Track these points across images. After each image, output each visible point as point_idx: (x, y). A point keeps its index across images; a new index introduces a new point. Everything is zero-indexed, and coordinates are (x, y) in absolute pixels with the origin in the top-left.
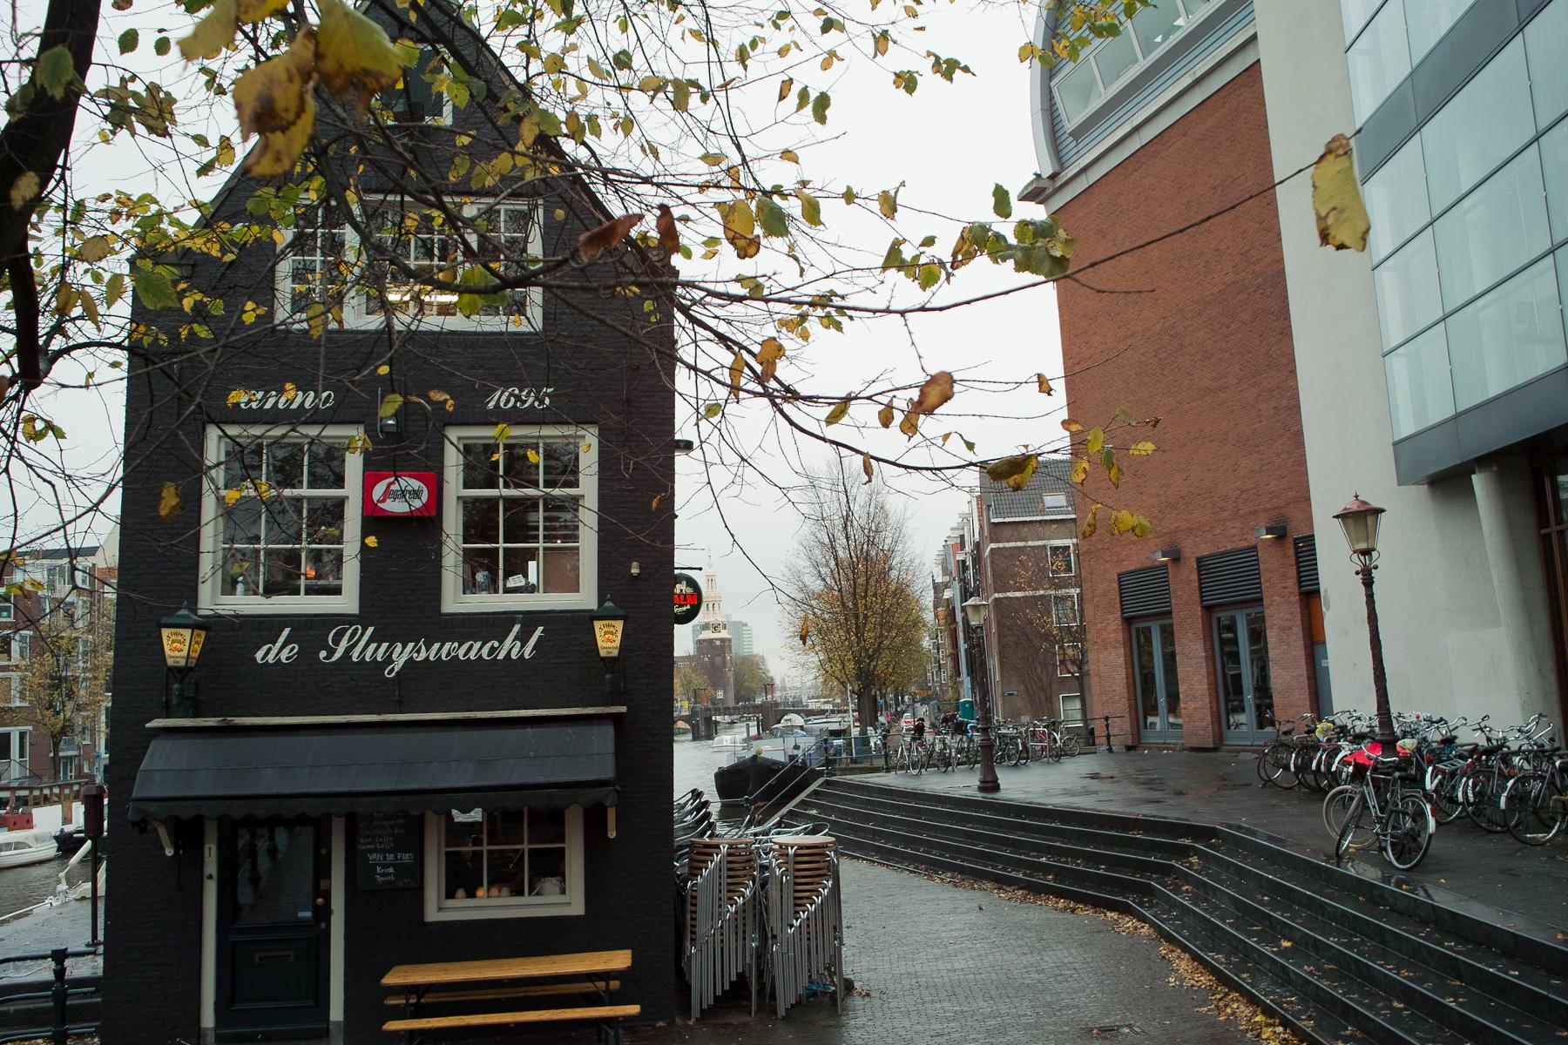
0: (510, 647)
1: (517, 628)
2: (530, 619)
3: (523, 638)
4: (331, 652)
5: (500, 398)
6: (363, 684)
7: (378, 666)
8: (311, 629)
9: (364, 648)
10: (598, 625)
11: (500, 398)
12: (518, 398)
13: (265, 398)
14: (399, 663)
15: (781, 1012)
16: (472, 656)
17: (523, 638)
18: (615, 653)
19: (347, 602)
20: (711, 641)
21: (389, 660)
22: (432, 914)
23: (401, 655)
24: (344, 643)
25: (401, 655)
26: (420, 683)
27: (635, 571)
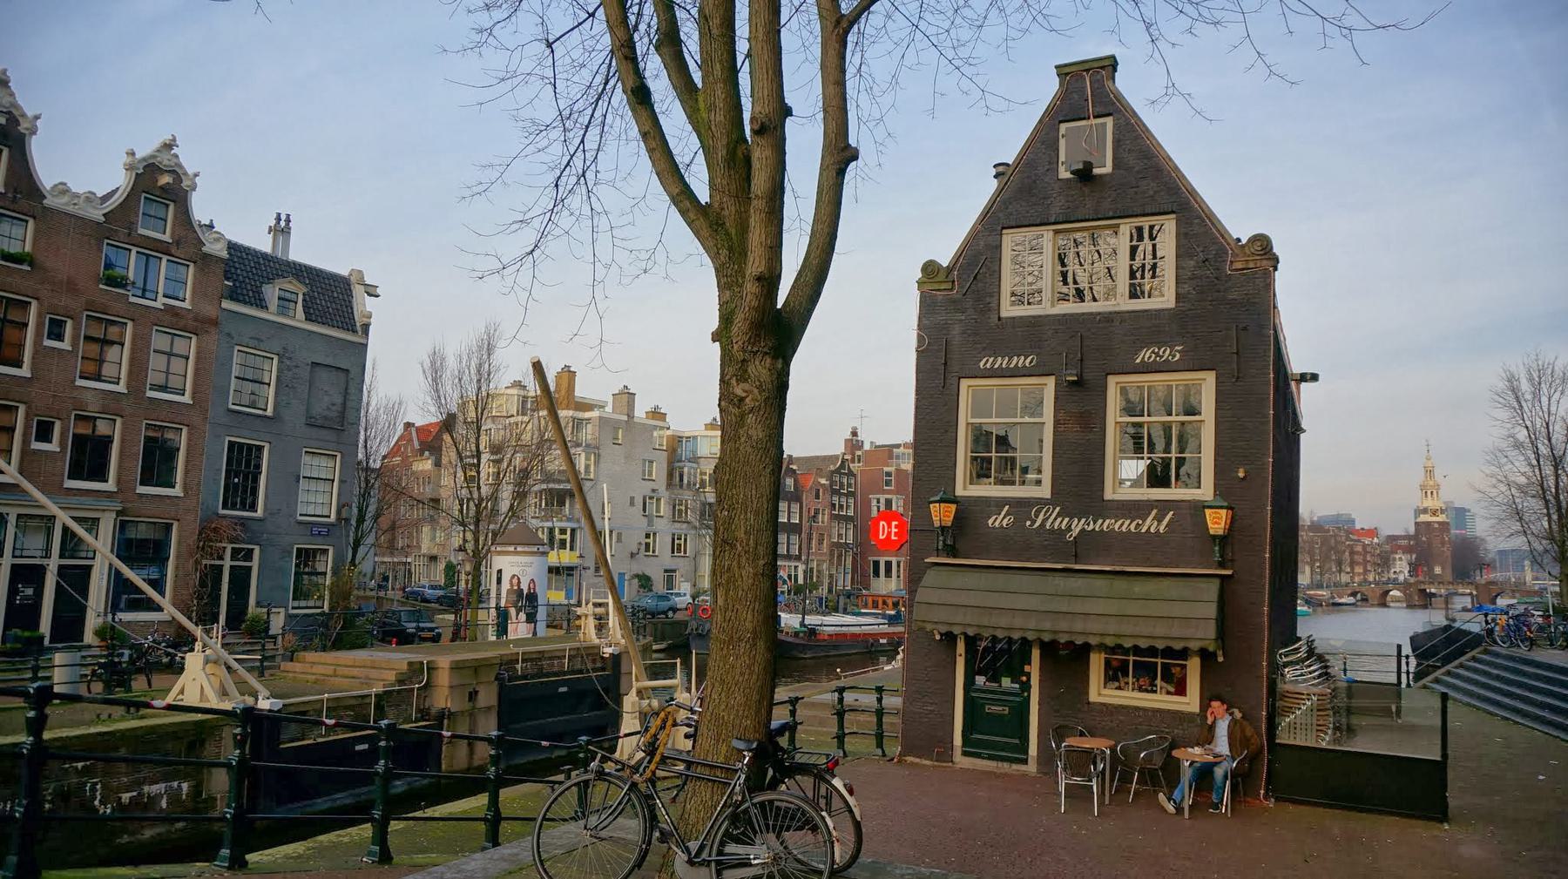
0: (1149, 524)
1: (1154, 512)
2: (1164, 506)
4: (1034, 522)
5: (1146, 355)
6: (1055, 543)
7: (1061, 533)
8: (1021, 507)
9: (1054, 520)
10: (1208, 512)
11: (1146, 355)
12: (1157, 355)
13: (994, 363)
14: (1075, 532)
15: (1036, 654)
16: (1124, 529)
18: (1221, 532)
19: (1045, 491)
20: (1429, 524)
21: (1069, 529)
22: (1093, 697)
23: (1077, 526)
24: (1041, 517)
25: (1077, 526)
26: (1086, 545)
27: (1241, 475)
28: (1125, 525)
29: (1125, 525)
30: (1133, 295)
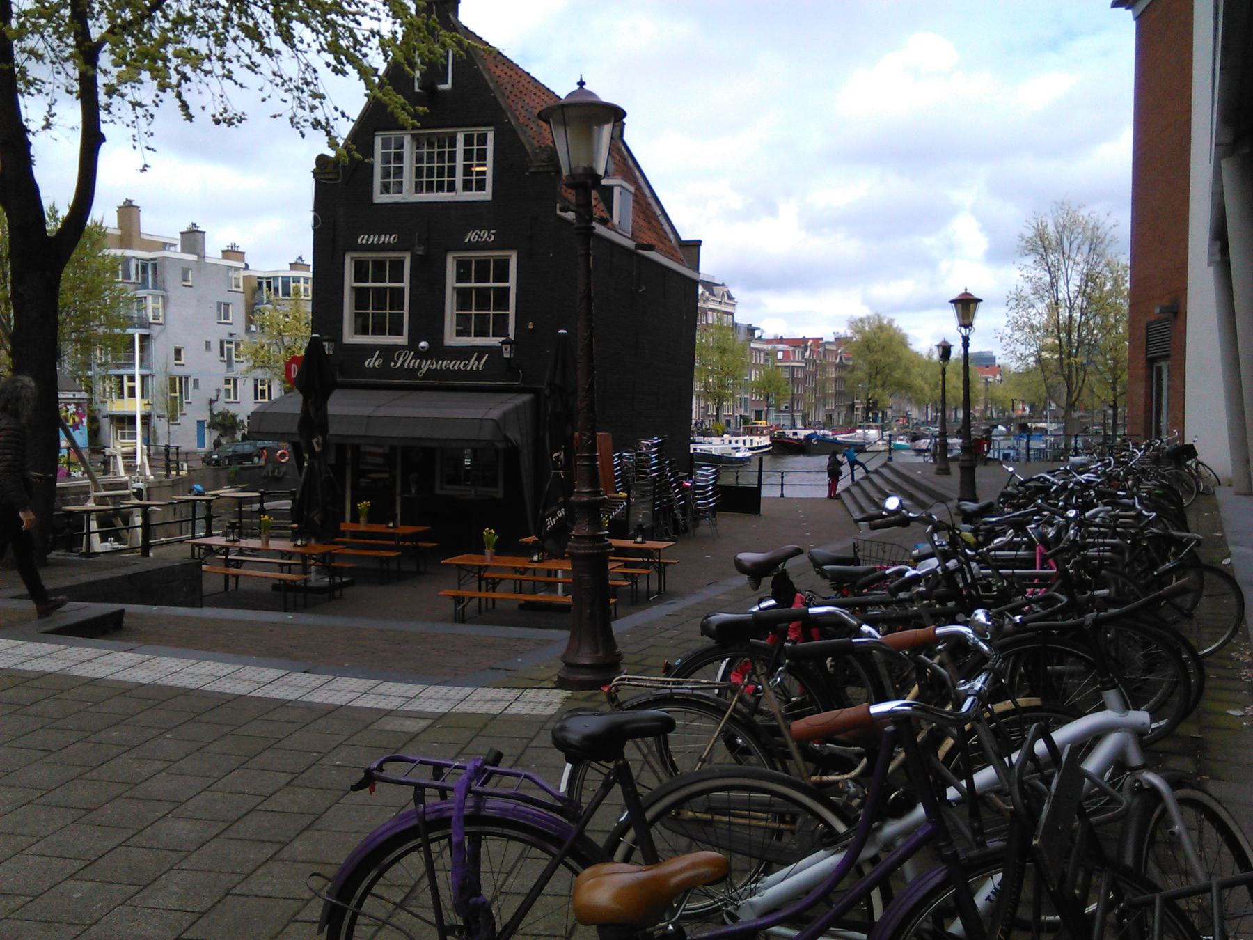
0: (473, 364)
2: (481, 350)
3: (479, 360)
5: (472, 236)
11: (472, 236)
17: (479, 360)
28: (457, 365)
29: (457, 365)
30: (467, 186)
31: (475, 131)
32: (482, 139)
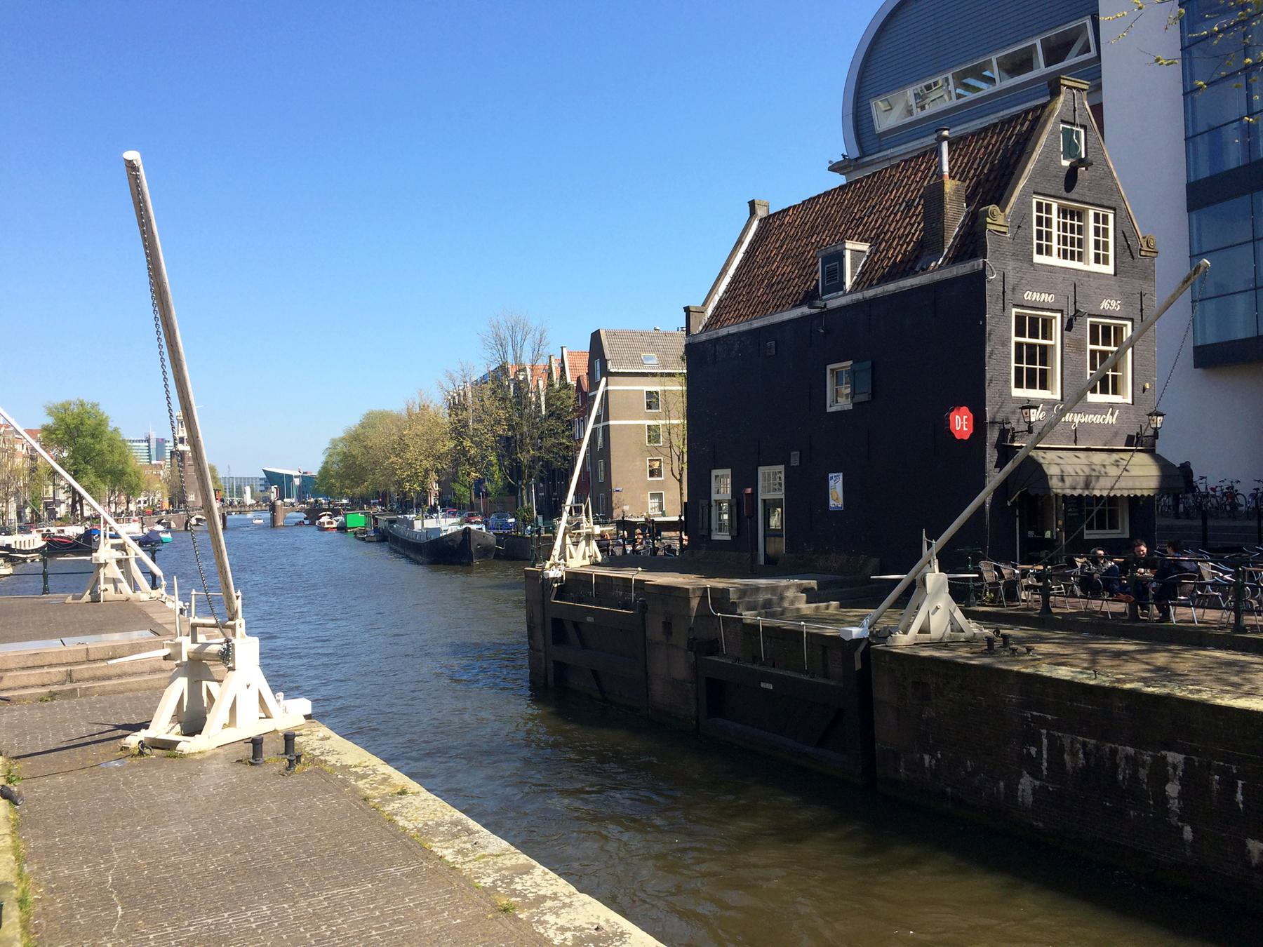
0: (1110, 419)
17: (1112, 414)
28: (1097, 419)
29: (1097, 419)
31: (1102, 212)
32: (1049, 210)
